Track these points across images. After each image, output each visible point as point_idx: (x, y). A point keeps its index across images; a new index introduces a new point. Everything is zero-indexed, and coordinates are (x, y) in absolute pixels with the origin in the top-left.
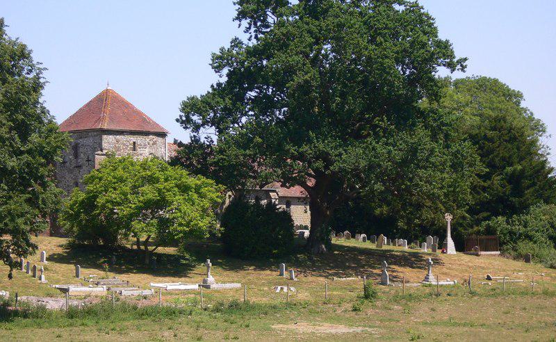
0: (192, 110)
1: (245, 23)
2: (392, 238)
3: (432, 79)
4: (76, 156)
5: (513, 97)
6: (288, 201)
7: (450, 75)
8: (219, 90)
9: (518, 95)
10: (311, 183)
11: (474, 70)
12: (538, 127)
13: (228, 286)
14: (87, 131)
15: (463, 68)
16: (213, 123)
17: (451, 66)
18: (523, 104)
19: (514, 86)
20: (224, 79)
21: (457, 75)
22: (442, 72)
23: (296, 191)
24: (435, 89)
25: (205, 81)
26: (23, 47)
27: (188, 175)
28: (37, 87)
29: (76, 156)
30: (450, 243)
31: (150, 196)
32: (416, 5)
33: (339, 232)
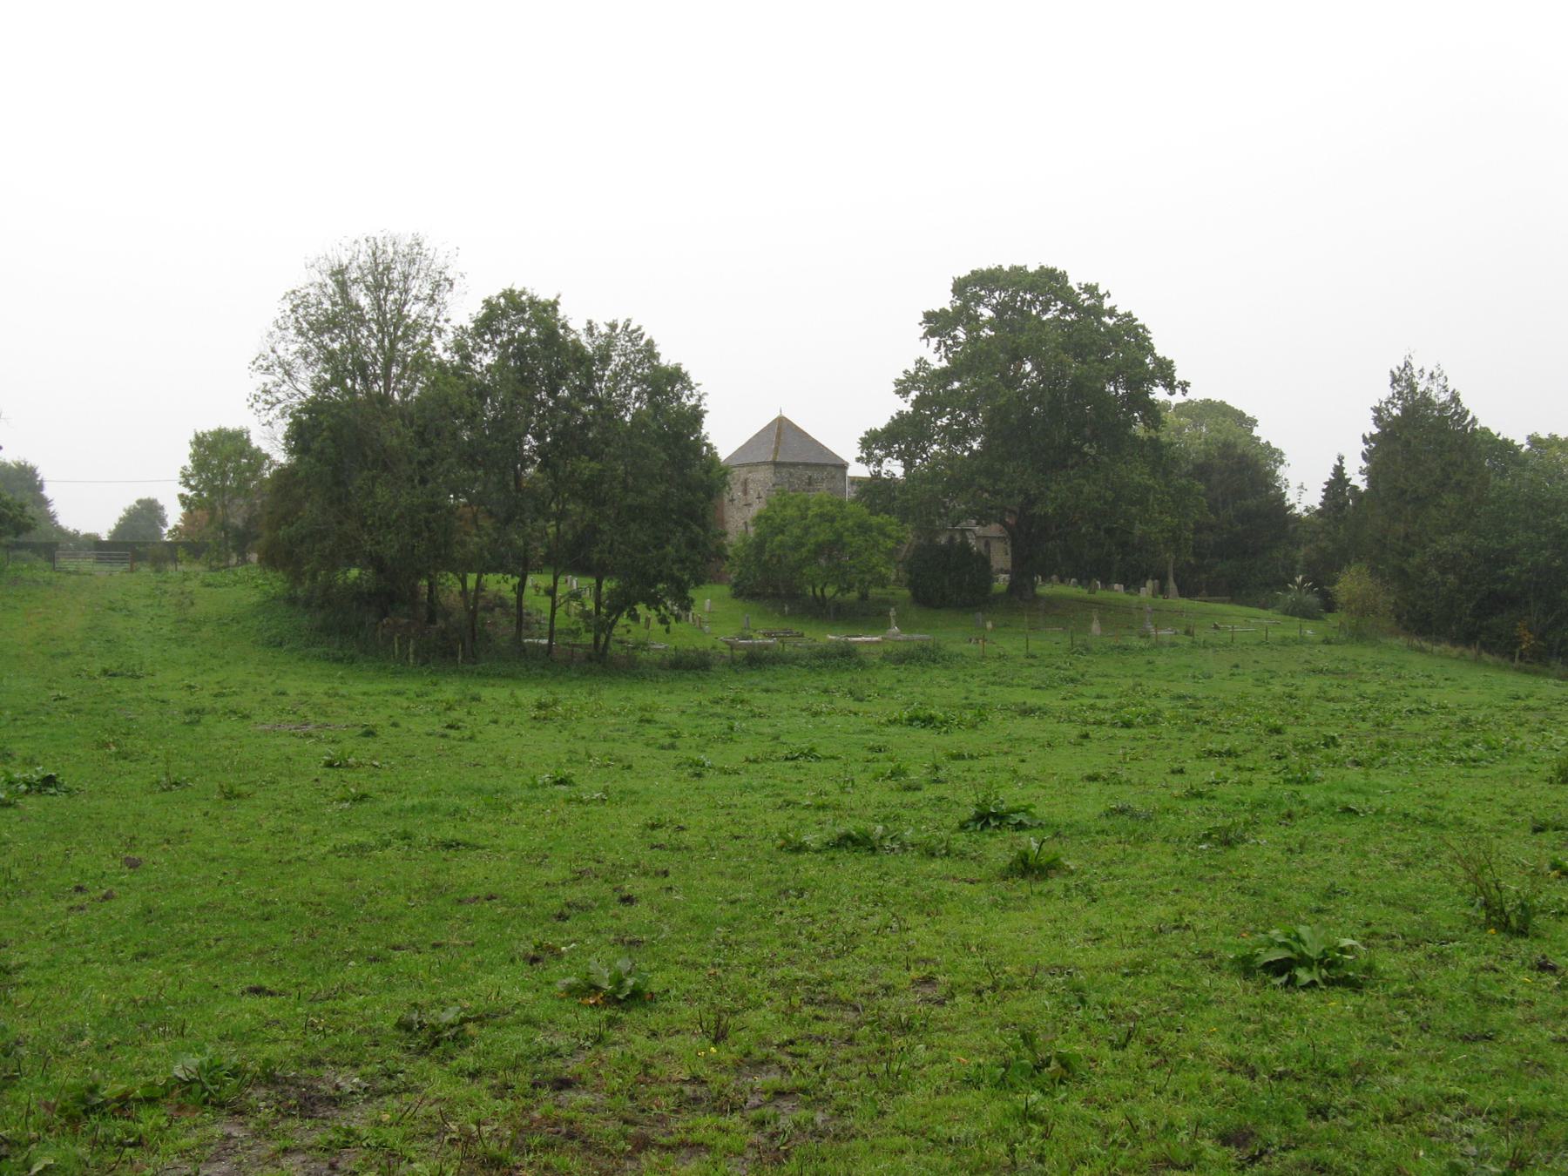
0: (873, 442)
1: (934, 341)
2: (1107, 583)
3: (1152, 403)
4: (745, 492)
5: (1244, 422)
6: (988, 542)
7: (1169, 398)
8: (901, 421)
9: (1254, 422)
10: (1010, 520)
11: (1196, 394)
12: (1276, 456)
13: (916, 636)
14: (758, 464)
15: (1184, 391)
16: (900, 456)
17: (1170, 387)
18: (1256, 432)
19: (544, 295)
20: (907, 408)
21: (1178, 398)
22: (1159, 394)
23: (994, 529)
24: (1153, 413)
25: (887, 407)
26: (678, 369)
27: (93, 1090)
28: (696, 416)
29: (745, 492)
30: (1172, 585)
31: (822, 537)
32: (1129, 315)
33: (1046, 578)
